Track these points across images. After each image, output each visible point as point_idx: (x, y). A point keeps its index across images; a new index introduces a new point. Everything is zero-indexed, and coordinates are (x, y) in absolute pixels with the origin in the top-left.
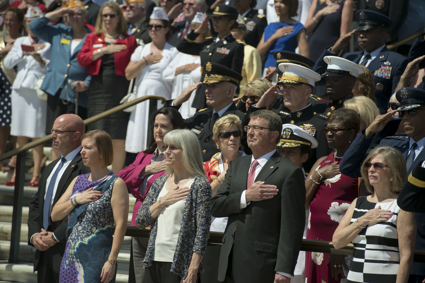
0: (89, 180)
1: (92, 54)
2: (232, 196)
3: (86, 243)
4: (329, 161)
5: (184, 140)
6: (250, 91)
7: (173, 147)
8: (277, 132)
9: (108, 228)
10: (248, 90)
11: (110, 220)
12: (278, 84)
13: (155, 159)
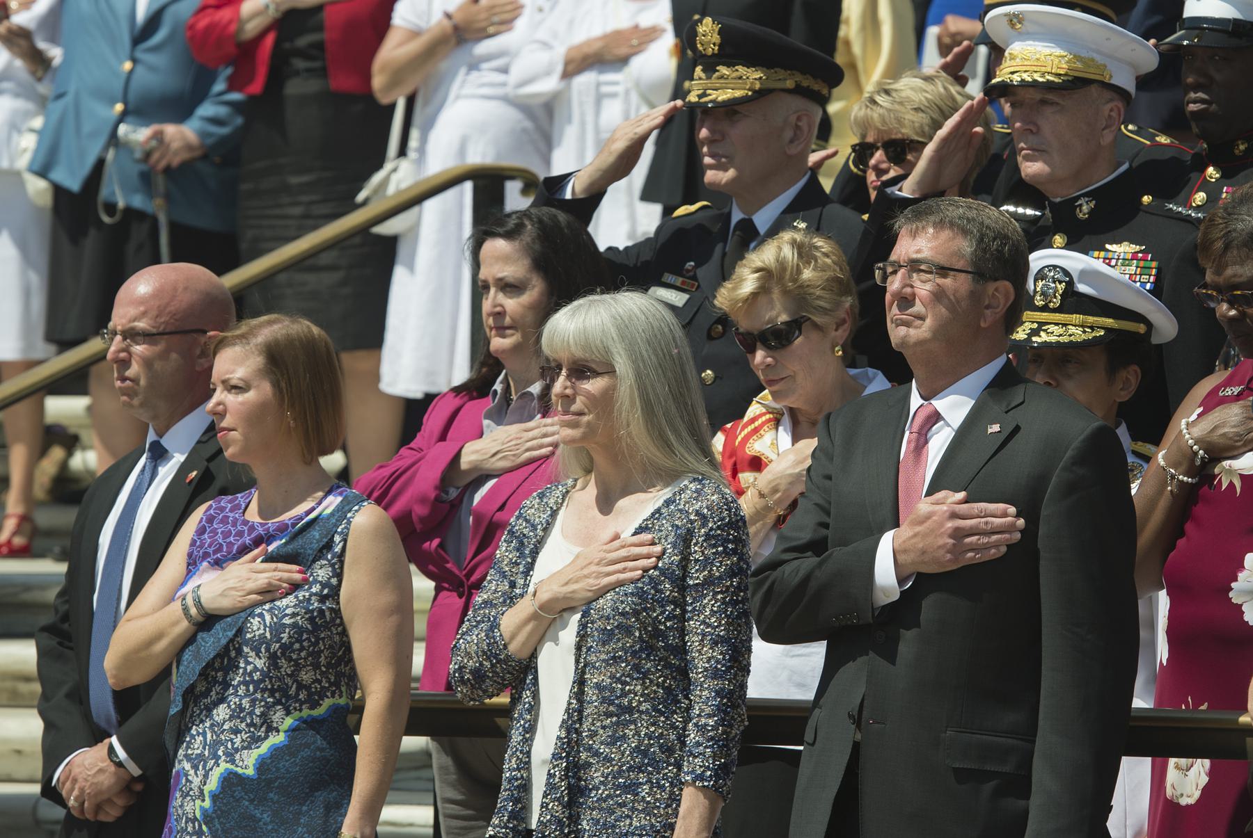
0: (248, 516)
1: (236, 17)
2: (838, 555)
3: (250, 772)
4: (1236, 390)
5: (622, 337)
6: (884, 122)
7: (581, 371)
8: (1007, 283)
9: (336, 710)
10: (875, 116)
11: (339, 675)
12: (995, 92)
13: (501, 415)
